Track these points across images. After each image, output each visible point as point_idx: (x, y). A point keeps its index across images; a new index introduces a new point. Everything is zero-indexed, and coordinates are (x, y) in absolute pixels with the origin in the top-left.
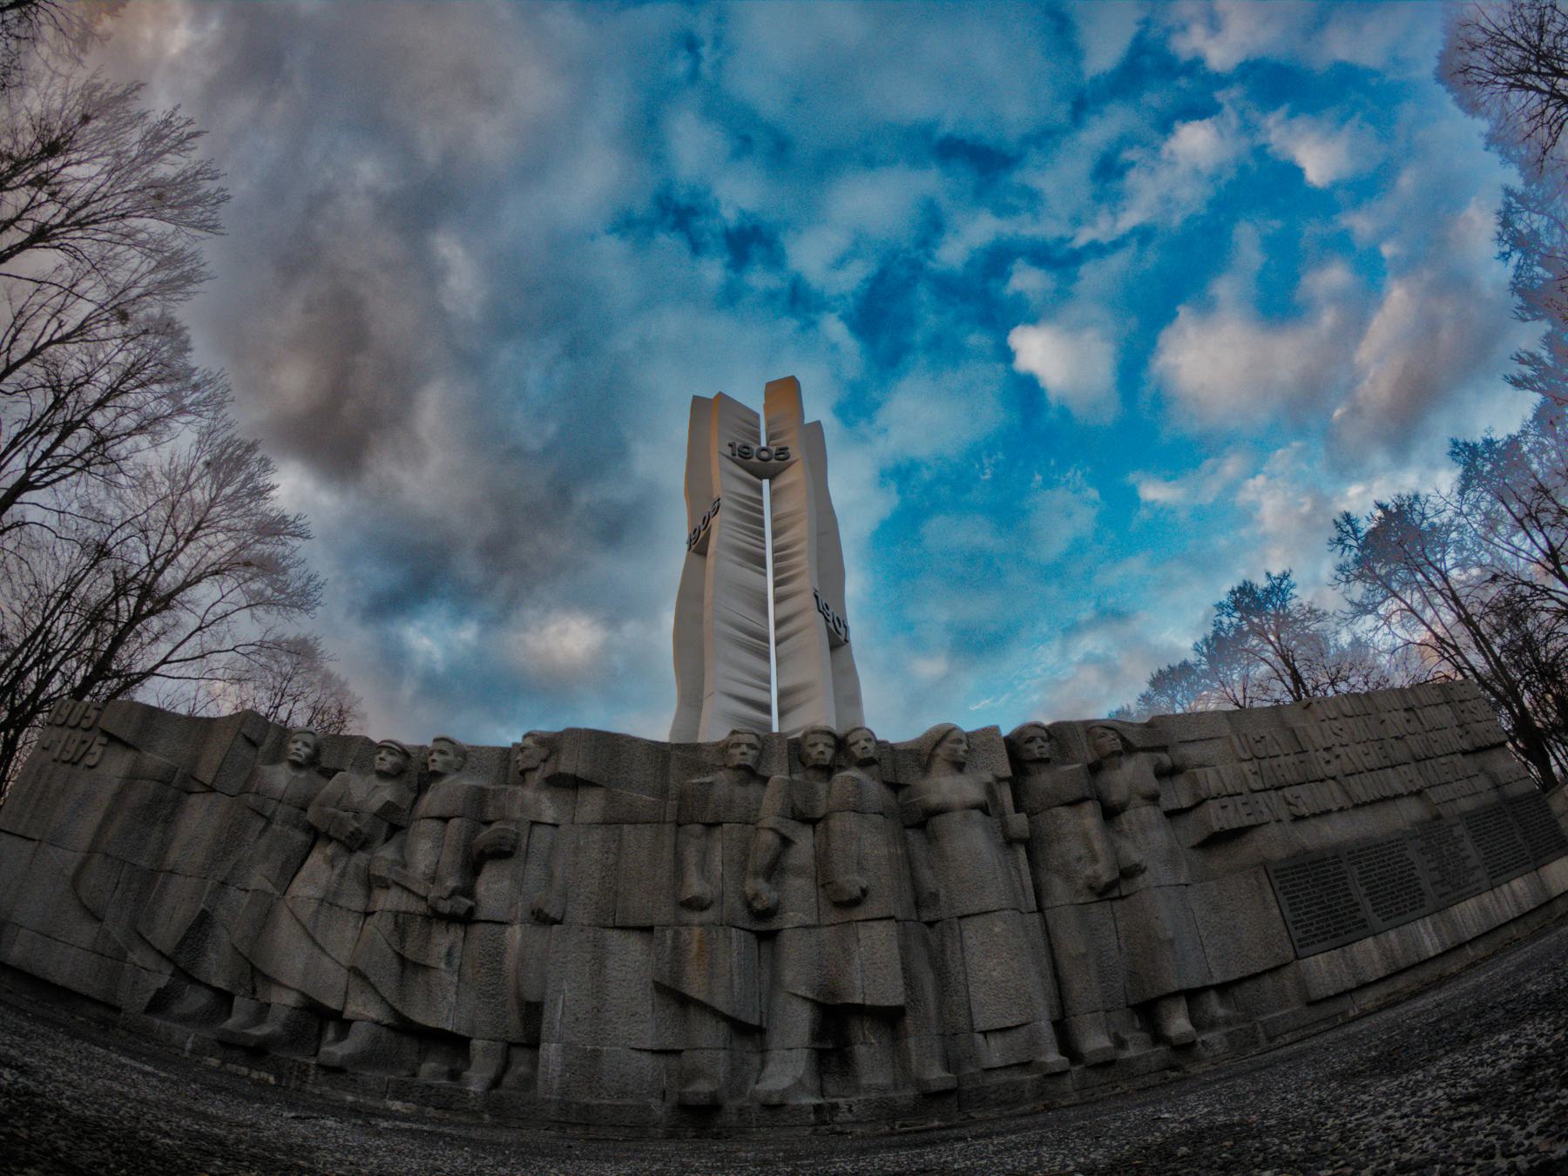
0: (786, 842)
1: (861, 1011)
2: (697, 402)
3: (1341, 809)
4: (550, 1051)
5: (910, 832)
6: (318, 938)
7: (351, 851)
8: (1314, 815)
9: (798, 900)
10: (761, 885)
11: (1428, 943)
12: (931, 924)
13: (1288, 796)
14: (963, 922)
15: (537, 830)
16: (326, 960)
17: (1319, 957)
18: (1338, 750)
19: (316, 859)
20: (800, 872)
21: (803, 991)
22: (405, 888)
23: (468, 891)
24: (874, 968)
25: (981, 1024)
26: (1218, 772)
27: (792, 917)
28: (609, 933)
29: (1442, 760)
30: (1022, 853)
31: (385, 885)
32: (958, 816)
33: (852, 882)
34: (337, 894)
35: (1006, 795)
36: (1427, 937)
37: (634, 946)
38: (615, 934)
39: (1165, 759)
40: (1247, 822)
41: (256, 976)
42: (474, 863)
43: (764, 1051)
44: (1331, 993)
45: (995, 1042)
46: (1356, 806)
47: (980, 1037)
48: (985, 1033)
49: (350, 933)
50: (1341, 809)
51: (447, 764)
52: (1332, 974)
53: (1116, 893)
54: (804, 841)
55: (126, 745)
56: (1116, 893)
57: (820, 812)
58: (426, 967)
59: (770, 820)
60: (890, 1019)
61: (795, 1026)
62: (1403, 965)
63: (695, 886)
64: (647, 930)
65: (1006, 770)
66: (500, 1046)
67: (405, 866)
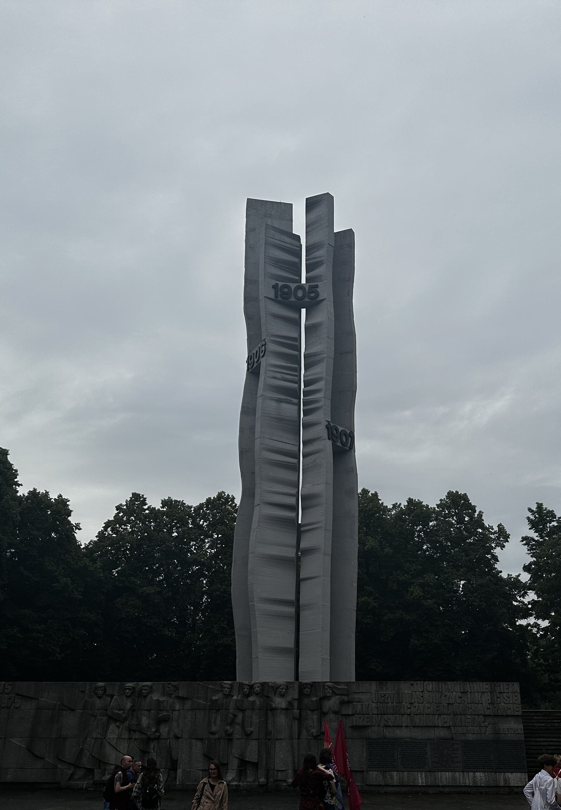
0: (235, 716)
1: (248, 762)
2: (251, 203)
3: (407, 727)
4: (179, 772)
5: (269, 711)
6: (118, 749)
7: (124, 722)
8: (394, 726)
9: (237, 731)
10: (228, 728)
11: (420, 781)
12: (269, 739)
13: (386, 718)
14: (276, 741)
15: (174, 712)
16: (120, 754)
17: (374, 772)
18: (416, 704)
19: (112, 727)
20: (238, 724)
21: (236, 755)
22: (140, 732)
23: (157, 731)
24: (252, 756)
25: (276, 769)
26: (362, 705)
27: (236, 736)
28: (193, 740)
29: (469, 717)
30: (296, 722)
31: (135, 731)
32: (279, 711)
33: (249, 729)
34: (121, 735)
35: (296, 704)
36: (421, 779)
37: (199, 744)
38: (194, 740)
39: (346, 698)
40: (365, 723)
41: (101, 763)
42: (160, 722)
43: (227, 769)
44: (374, 784)
45: (279, 773)
46: (414, 727)
47: (276, 772)
48: (278, 771)
49: (126, 745)
50: (407, 727)
51: (147, 693)
52: (376, 778)
53: (319, 738)
54: (240, 716)
55: (31, 698)
56: (319, 738)
57: (244, 709)
58: (149, 752)
59: (231, 711)
60: (256, 765)
61: (234, 763)
62: (405, 784)
63: (214, 729)
64: (201, 739)
65: (296, 697)
66: (167, 770)
67: (140, 725)
